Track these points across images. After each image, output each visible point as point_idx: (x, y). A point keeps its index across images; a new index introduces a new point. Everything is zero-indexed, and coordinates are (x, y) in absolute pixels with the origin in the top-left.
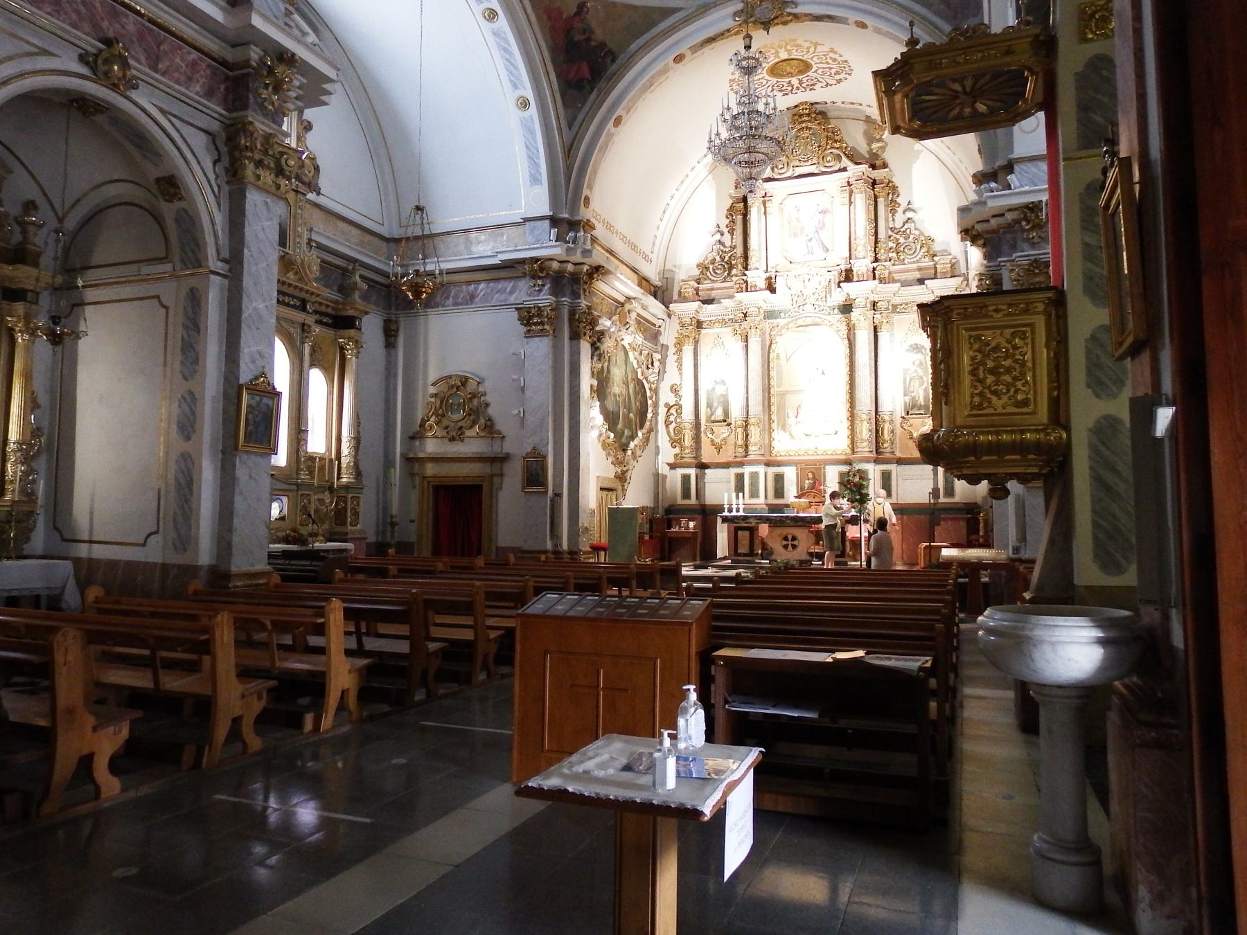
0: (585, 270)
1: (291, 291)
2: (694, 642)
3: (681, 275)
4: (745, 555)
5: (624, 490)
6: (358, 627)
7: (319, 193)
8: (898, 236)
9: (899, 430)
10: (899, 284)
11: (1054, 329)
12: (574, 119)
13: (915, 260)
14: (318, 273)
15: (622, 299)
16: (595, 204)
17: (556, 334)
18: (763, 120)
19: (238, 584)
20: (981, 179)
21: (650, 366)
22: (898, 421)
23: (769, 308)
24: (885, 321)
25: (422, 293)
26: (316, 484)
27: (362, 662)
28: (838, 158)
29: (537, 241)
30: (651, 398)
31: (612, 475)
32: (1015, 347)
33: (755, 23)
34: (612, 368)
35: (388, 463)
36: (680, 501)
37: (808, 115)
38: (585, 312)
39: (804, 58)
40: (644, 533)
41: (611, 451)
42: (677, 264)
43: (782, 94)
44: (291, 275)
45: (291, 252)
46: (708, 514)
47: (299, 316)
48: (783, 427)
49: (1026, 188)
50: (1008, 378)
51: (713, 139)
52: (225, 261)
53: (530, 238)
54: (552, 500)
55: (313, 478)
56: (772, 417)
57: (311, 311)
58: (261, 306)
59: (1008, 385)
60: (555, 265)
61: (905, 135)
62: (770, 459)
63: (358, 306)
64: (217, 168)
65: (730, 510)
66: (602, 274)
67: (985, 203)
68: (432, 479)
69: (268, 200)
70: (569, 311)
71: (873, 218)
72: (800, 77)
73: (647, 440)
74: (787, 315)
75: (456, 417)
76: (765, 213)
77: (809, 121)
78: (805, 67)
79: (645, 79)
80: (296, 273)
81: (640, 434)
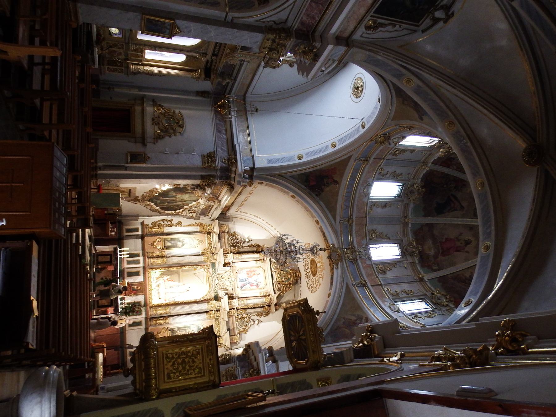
0: (232, 182)
1: (221, 50)
2: (38, 230)
3: (231, 225)
4: (97, 260)
5: (129, 201)
6: (47, 64)
7: (264, 67)
8: (248, 318)
9: (161, 327)
10: (227, 320)
11: (202, 386)
12: (294, 178)
13: (238, 326)
14: (230, 63)
15: (220, 199)
16: (260, 187)
17: (203, 169)
18: (293, 257)
19: (71, 6)
20: (270, 349)
21: (190, 212)
22: (166, 326)
23: (216, 264)
24: (211, 316)
25: (220, 108)
26: (129, 52)
27: (25, 63)
28: (279, 290)
29: (244, 161)
30: (175, 213)
31: (137, 195)
32: (194, 370)
33: (330, 252)
34: (188, 194)
35: (141, 88)
36: (125, 228)
37: (296, 276)
38: (213, 182)
39: (317, 273)
40: (108, 211)
41: (149, 194)
42: (236, 223)
43: (304, 265)
44: (228, 51)
45: (238, 52)
46: (119, 241)
47: (210, 52)
48: (163, 274)
49: (266, 369)
50: (180, 368)
51: (286, 236)
52: (232, 20)
53: (245, 158)
54: (123, 166)
55: (132, 51)
56: (167, 269)
57: (212, 58)
58: (212, 34)
59: (177, 369)
60: (234, 169)
61: (284, 314)
62: (147, 269)
63: (215, 80)
64: (272, 22)
65: (120, 251)
66: (230, 190)
67: (260, 352)
68: (133, 108)
69: (259, 43)
70: (214, 175)
71: (255, 306)
72: (310, 272)
73: (155, 211)
74: (214, 272)
75: (164, 122)
76: (257, 260)
77: (294, 277)
78: (314, 274)
79: (310, 208)
80: (229, 53)
81: (158, 208)
